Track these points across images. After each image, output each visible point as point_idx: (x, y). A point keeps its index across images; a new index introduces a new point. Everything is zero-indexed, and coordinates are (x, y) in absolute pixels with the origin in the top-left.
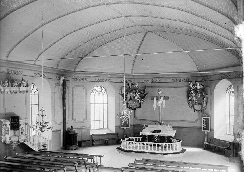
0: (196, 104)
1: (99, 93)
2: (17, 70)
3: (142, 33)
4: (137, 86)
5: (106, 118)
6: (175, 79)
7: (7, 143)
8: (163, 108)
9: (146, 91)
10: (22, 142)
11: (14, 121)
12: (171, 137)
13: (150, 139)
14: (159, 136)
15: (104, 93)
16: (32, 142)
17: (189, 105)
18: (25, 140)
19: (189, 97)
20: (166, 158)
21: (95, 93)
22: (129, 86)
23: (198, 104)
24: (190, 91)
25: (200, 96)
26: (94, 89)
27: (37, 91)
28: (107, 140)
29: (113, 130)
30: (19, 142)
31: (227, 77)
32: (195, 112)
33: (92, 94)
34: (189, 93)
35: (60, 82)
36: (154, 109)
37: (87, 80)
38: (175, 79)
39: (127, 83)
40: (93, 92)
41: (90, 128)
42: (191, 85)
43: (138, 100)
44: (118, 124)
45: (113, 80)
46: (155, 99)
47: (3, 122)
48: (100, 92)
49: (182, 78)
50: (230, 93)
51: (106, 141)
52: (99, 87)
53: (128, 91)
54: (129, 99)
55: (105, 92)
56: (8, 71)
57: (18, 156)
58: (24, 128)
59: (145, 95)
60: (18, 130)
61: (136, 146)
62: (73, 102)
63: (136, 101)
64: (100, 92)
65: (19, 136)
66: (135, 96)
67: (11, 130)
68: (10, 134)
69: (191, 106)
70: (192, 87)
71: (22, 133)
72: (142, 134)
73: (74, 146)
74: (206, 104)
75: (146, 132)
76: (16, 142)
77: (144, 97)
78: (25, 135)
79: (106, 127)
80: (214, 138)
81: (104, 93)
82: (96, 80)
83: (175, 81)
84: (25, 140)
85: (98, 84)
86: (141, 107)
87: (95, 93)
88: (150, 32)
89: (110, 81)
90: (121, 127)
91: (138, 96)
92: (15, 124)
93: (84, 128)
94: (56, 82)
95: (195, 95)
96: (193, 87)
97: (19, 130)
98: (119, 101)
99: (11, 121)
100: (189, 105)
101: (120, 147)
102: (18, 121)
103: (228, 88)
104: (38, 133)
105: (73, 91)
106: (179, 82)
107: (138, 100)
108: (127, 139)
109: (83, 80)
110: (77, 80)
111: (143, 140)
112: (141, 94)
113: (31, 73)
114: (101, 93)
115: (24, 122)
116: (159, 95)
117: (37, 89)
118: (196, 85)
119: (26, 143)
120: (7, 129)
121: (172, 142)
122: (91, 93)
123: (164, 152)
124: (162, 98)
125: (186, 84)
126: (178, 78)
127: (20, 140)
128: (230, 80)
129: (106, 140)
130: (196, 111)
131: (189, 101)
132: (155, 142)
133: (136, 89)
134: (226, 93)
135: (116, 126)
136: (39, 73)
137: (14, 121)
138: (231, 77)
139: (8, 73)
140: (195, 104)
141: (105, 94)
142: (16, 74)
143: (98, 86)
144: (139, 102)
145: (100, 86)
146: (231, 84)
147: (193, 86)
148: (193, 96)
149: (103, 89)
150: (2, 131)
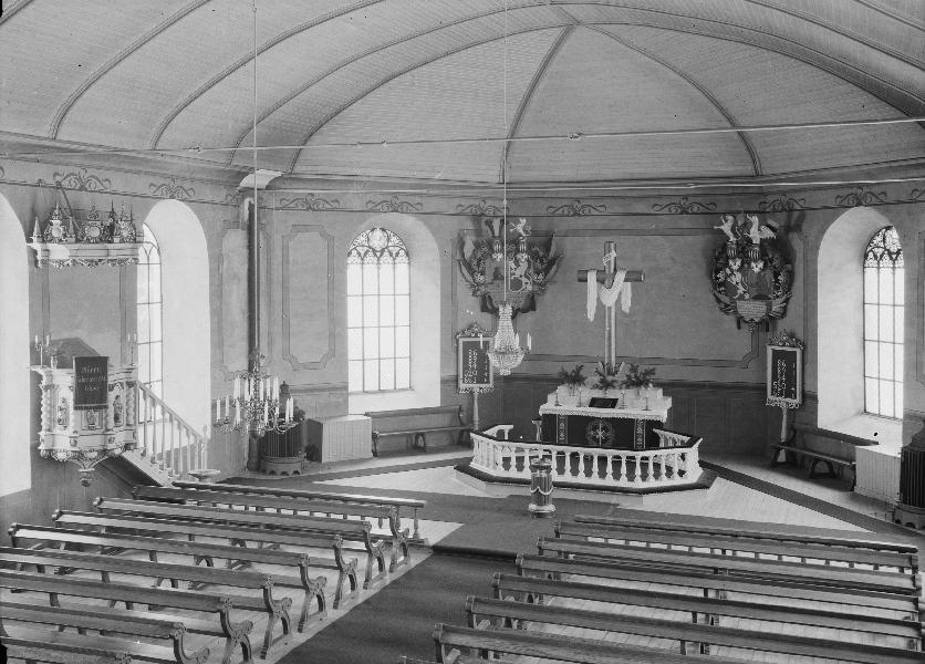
0: (747, 296)
1: (378, 254)
2: (91, 172)
3: (550, 31)
4: (520, 228)
5: (403, 351)
6: (665, 202)
7: (61, 456)
8: (623, 313)
9: (553, 248)
10: (117, 452)
11: (86, 375)
12: (658, 424)
13: (579, 430)
14: (613, 420)
15: (397, 254)
16: (150, 452)
17: (719, 301)
18: (127, 447)
19: (717, 271)
20: (651, 504)
21: (362, 253)
22: (493, 233)
23: (756, 298)
24: (724, 247)
25: (762, 270)
26: (362, 239)
27: (155, 251)
28: (422, 434)
29: (429, 395)
30: (104, 451)
31: (185, 196)
32: (739, 328)
33: (353, 259)
34: (717, 259)
35: (238, 216)
36: (591, 315)
37: (336, 205)
38: (665, 202)
39: (477, 218)
40: (354, 252)
41: (346, 388)
42: (726, 228)
43: (524, 280)
44: (453, 373)
45: (431, 205)
46: (592, 277)
47: (44, 378)
48: (382, 251)
49: (691, 199)
50: (881, 256)
51: (417, 438)
52: (378, 233)
53: (485, 247)
54: (489, 278)
55: (402, 253)
56: (58, 178)
57: (101, 510)
58: (123, 400)
59: (552, 263)
60: (100, 408)
61: (517, 458)
62: (285, 288)
63: (517, 284)
64: (382, 251)
65: (107, 430)
66: (513, 266)
67: (76, 408)
68: (71, 424)
69: (727, 305)
70: (521, 231)
71: (116, 418)
72: (547, 412)
73: (295, 459)
74: (784, 298)
75: (565, 402)
76: (94, 454)
77: (547, 271)
78: (128, 425)
79: (403, 383)
80: (819, 426)
81: (397, 254)
82: (370, 206)
83: (560, 212)
84: (127, 447)
85: (375, 218)
86: (534, 310)
87: (362, 253)
88: (586, 25)
89: (336, 205)
90: (462, 386)
91: (524, 266)
92: (94, 385)
93: (329, 389)
94: (229, 214)
95: (742, 263)
96: (735, 235)
97: (106, 407)
98: (453, 283)
99: (79, 374)
100: (719, 301)
101: (471, 459)
102: (104, 373)
103: (872, 238)
104: (159, 408)
105: (285, 248)
106: (681, 213)
107: (524, 280)
108: (493, 431)
109: (586, 212)
110: (673, 211)
111: (549, 438)
112: (534, 256)
113: (141, 184)
114: (386, 253)
115: (123, 376)
116: (609, 263)
117: (155, 244)
118: (747, 225)
119: (128, 455)
120: (60, 403)
121: (662, 444)
122: (350, 254)
123: (639, 484)
124: (621, 276)
125: (701, 222)
126: (676, 200)
127: (110, 446)
128: (887, 211)
129: (418, 435)
130: (743, 325)
131: (721, 285)
132: (597, 443)
133: (514, 241)
134: (866, 256)
135: (444, 382)
136: (167, 181)
137: (86, 375)
138: (892, 197)
139: (59, 186)
140: (742, 298)
141: (402, 258)
142: (86, 190)
143: (373, 230)
144: (530, 288)
145: (383, 230)
146: (886, 223)
147: (733, 230)
148: (735, 268)
149: (394, 240)
150: (41, 420)
